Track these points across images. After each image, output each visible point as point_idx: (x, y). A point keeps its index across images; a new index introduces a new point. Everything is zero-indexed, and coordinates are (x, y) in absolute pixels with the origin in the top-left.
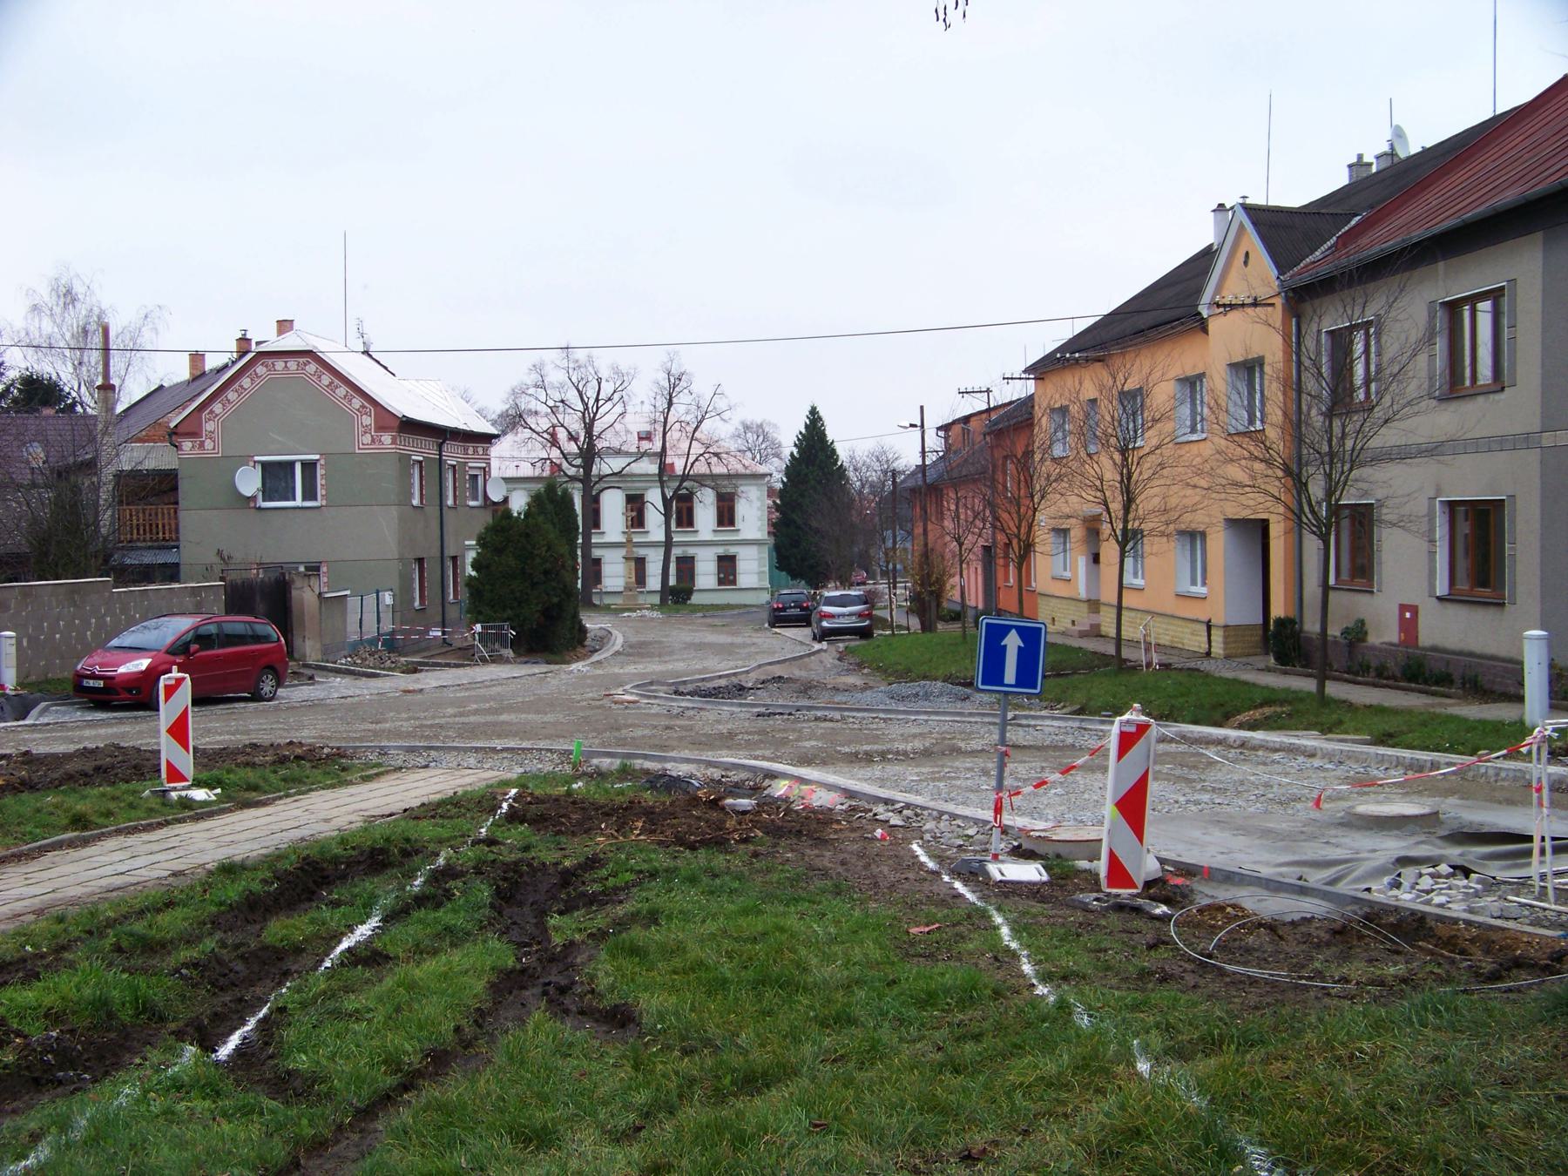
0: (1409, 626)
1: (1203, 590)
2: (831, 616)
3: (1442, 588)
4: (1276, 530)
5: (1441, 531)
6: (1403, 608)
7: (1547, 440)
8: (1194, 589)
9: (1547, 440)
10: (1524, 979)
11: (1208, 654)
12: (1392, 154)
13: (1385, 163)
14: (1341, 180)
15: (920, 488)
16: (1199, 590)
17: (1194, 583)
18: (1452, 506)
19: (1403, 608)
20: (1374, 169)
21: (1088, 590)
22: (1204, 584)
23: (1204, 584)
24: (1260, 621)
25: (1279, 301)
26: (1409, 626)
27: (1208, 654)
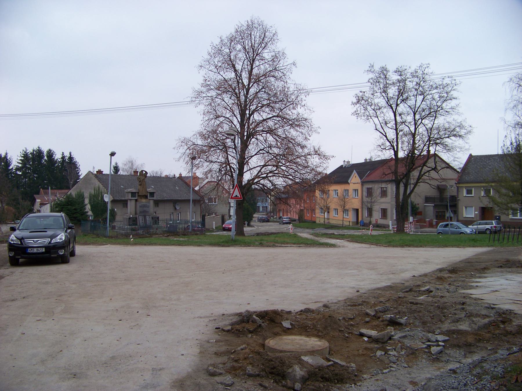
0: (377, 221)
1: (337, 216)
2: (285, 221)
3: (380, 217)
4: (360, 210)
5: (380, 212)
6: (376, 219)
7: (391, 203)
8: (346, 217)
9: (391, 203)
10: (385, 138)
11: (349, 225)
12: (371, 159)
13: (370, 161)
14: (363, 161)
15: (190, 177)
16: (336, 216)
17: (336, 215)
18: (381, 209)
19: (376, 219)
20: (368, 161)
21: (327, 217)
22: (337, 215)
23: (337, 215)
24: (356, 221)
25: (360, 183)
26: (377, 221)
27: (349, 225)
